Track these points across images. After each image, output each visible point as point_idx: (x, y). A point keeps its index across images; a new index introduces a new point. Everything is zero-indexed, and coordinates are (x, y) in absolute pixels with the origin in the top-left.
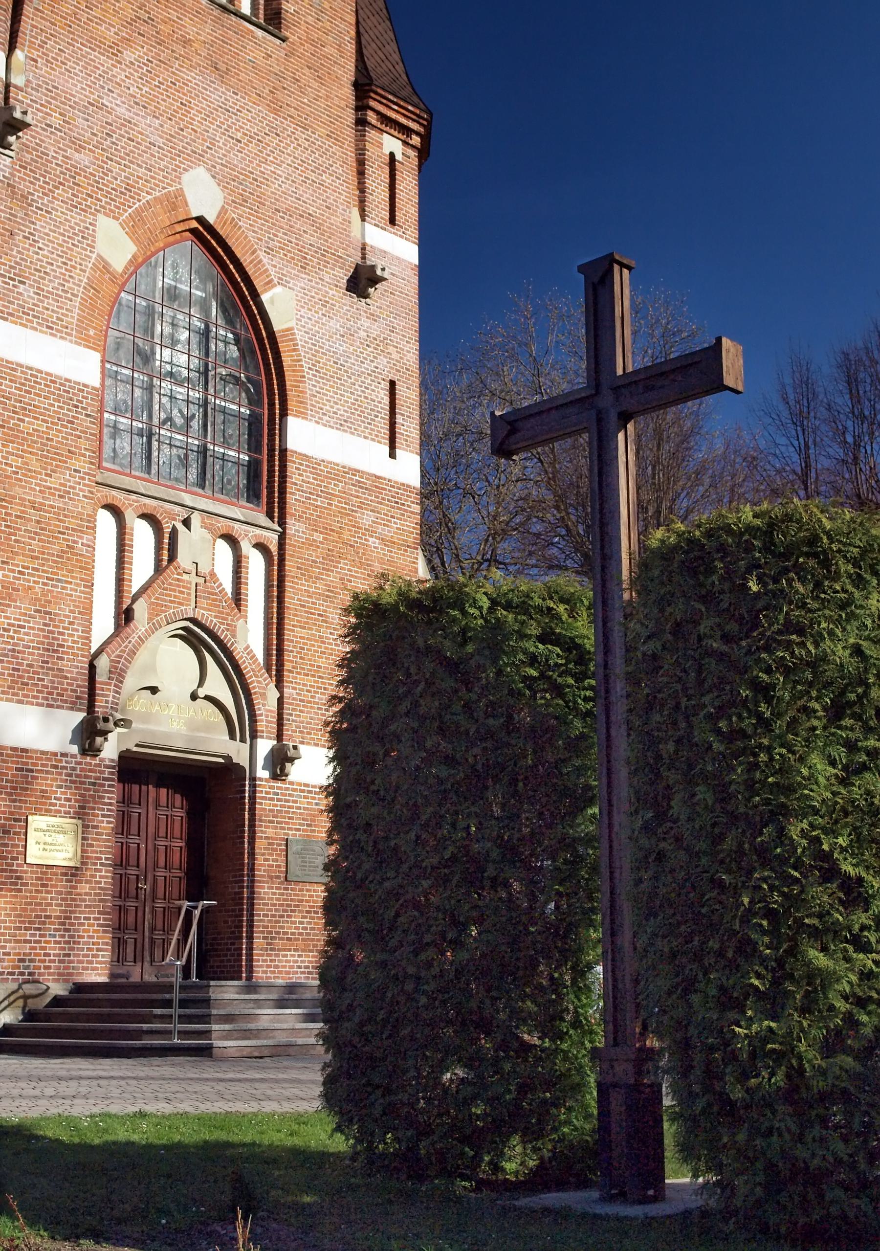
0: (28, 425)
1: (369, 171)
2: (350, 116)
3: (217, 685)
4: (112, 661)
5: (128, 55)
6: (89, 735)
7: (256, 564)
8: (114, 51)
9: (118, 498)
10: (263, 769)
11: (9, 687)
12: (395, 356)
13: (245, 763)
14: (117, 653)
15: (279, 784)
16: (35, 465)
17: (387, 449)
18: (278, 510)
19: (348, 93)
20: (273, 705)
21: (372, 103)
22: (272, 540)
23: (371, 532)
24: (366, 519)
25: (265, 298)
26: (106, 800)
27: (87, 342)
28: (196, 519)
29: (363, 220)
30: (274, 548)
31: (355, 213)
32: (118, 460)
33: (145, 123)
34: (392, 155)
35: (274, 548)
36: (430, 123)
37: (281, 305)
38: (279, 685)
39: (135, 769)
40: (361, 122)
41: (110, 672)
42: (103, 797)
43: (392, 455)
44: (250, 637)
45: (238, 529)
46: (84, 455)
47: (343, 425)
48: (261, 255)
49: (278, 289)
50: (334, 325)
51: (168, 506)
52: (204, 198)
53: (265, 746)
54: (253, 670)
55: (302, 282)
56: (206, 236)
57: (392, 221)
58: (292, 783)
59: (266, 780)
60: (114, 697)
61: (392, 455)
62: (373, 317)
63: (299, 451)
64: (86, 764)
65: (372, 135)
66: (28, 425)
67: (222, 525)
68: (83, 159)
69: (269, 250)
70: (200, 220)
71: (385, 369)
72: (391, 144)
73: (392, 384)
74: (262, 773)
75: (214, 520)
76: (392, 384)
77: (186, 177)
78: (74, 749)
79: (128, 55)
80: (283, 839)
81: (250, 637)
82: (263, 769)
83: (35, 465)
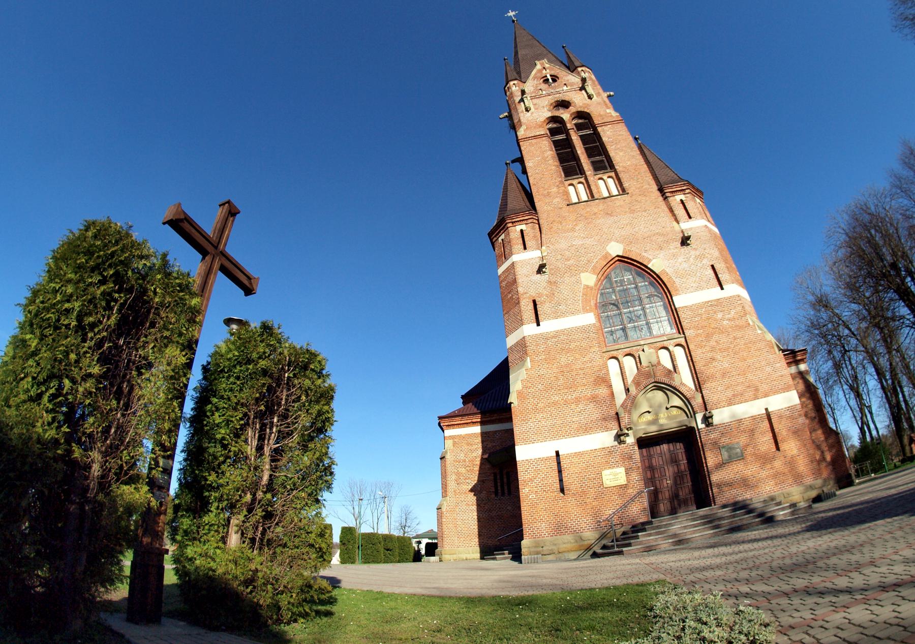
0: (573, 346)
1: (674, 209)
2: (661, 199)
3: (676, 401)
5: (577, 228)
6: (619, 437)
7: (679, 353)
8: (573, 230)
9: (614, 353)
16: (578, 356)
17: (719, 288)
19: (658, 193)
20: (700, 400)
22: (682, 341)
24: (720, 315)
27: (587, 311)
28: (646, 348)
30: (684, 343)
31: (675, 223)
32: (630, 339)
33: (588, 242)
34: (682, 201)
35: (684, 343)
36: (689, 183)
37: (656, 265)
38: (701, 392)
39: (644, 443)
40: (665, 198)
43: (722, 289)
44: (685, 379)
45: (666, 344)
47: (699, 288)
48: (644, 254)
49: (654, 261)
50: (680, 259)
52: (616, 249)
53: (699, 417)
55: (662, 254)
56: (624, 260)
57: (690, 217)
61: (722, 289)
65: (670, 199)
66: (573, 346)
67: (659, 345)
68: (571, 262)
70: (618, 256)
71: (707, 263)
72: (679, 197)
73: (712, 266)
74: (701, 426)
75: (655, 345)
76: (712, 266)
77: (608, 248)
78: (616, 443)
79: (577, 228)
81: (685, 379)
83: (578, 356)
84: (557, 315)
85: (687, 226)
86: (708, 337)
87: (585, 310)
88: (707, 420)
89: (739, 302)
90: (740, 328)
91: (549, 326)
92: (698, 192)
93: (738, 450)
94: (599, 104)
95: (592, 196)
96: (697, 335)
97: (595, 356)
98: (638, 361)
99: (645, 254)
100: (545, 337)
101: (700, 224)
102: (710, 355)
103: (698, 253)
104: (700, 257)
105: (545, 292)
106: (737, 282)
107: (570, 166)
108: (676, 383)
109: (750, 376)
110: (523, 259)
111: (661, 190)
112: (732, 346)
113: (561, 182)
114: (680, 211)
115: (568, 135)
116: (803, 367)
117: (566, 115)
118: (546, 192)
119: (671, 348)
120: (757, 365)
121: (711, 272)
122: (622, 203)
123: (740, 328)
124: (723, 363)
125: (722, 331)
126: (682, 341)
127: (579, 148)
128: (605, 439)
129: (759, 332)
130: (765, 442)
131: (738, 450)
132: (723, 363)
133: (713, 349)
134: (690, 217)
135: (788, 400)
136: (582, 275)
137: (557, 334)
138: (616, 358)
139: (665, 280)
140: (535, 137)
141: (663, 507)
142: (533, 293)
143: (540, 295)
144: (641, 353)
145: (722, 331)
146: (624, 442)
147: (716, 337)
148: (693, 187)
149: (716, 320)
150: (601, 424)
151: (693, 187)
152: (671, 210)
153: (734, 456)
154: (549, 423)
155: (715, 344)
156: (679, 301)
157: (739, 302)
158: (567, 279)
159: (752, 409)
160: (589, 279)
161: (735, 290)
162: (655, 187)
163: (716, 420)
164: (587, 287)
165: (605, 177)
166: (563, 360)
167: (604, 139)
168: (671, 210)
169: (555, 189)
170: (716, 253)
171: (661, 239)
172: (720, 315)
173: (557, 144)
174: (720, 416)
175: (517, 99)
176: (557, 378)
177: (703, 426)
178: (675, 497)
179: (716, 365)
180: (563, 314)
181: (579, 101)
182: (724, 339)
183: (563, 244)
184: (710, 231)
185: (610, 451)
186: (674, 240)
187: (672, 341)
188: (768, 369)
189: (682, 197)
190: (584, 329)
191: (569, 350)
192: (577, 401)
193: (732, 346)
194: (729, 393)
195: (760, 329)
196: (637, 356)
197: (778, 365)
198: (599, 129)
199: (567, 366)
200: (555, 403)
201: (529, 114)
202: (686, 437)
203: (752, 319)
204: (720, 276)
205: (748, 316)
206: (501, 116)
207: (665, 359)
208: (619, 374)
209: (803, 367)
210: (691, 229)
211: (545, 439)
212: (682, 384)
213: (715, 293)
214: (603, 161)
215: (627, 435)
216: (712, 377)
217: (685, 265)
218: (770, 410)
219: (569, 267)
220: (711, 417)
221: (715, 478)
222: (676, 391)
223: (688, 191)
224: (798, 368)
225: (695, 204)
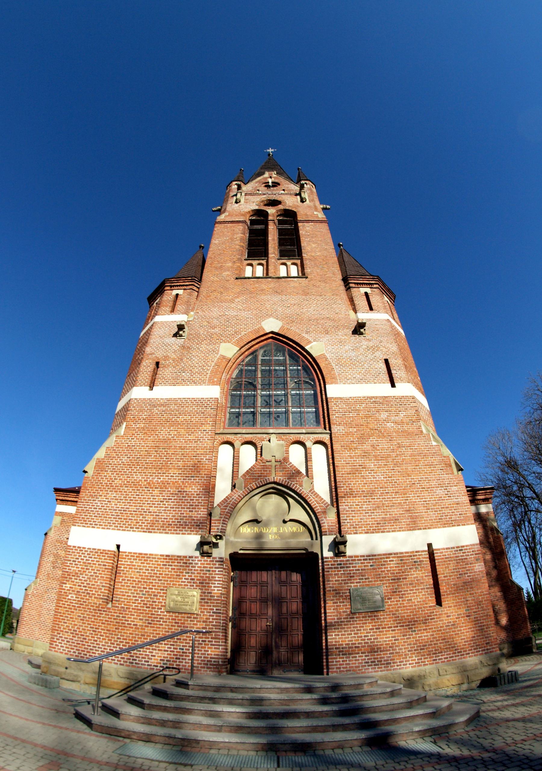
0: (181, 419)
4: (221, 509)
6: (205, 547)
7: (319, 454)
9: (231, 438)
10: (329, 551)
11: (161, 527)
12: (384, 350)
13: (317, 550)
14: (225, 504)
15: (342, 559)
18: (328, 424)
19: (342, 283)
21: (350, 281)
23: (387, 420)
24: (384, 415)
25: (307, 348)
26: (217, 579)
27: (213, 383)
29: (356, 312)
30: (328, 442)
31: (352, 313)
33: (244, 314)
34: (366, 294)
35: (328, 442)
36: (378, 277)
41: (221, 514)
42: (215, 577)
44: (320, 486)
45: (302, 438)
46: (209, 424)
47: (363, 380)
51: (259, 436)
52: (272, 325)
53: (328, 540)
54: (316, 501)
56: (278, 338)
57: (371, 309)
58: (350, 557)
59: (331, 558)
60: (222, 526)
61: (393, 385)
62: (369, 340)
63: (334, 396)
64: (204, 561)
65: (353, 290)
66: (181, 419)
67: (293, 438)
69: (307, 333)
70: (272, 332)
71: (381, 356)
72: (363, 290)
73: (386, 361)
74: (327, 554)
75: (287, 436)
76: (386, 361)
78: (197, 554)
80: (347, 589)
82: (329, 551)
84: (176, 382)
85: (363, 316)
86: (363, 439)
87: (212, 382)
88: (338, 546)
89: (413, 404)
90: (408, 434)
91: (162, 392)
92: (387, 291)
93: (378, 597)
94: (309, 207)
95: (267, 274)
96: (348, 434)
97: (204, 436)
98: (260, 452)
99: (306, 336)
100: (153, 403)
101: (381, 317)
102: (360, 461)
103: (371, 344)
104: (375, 349)
105: (174, 356)
106: (416, 385)
107: (256, 248)
108: (304, 490)
109: (413, 498)
110: (165, 319)
111: (345, 280)
112: (394, 454)
113: (240, 260)
114: (361, 302)
115: (267, 225)
116: (483, 509)
117: (271, 211)
118: (219, 265)
119: (308, 444)
120: (425, 484)
121: (384, 367)
122: (297, 285)
123: (408, 434)
124: (376, 474)
125: (382, 434)
126: (326, 438)
127: (273, 237)
128: (186, 543)
129: (434, 443)
130: (420, 596)
131: (378, 597)
132: (376, 474)
133: (366, 455)
134: (371, 309)
135: (469, 535)
136: (223, 345)
137: (168, 402)
138: (231, 444)
139: (322, 365)
140: (232, 222)
141: (250, 659)
142: (159, 355)
143: (166, 358)
144: (265, 443)
145: (382, 434)
146: (208, 555)
147: (373, 440)
148: (384, 284)
149: (377, 420)
150: (182, 526)
151: (384, 284)
152: (352, 300)
153: (367, 609)
154: (120, 506)
155: (369, 448)
156: (333, 391)
157: (413, 404)
158: (204, 347)
159: (407, 542)
160: (229, 350)
161: (408, 389)
162: (340, 277)
163: (350, 551)
164: (224, 357)
165: (289, 263)
166: (163, 433)
167: (301, 232)
168: (352, 300)
169: (230, 264)
170: (394, 348)
171: (329, 323)
172: (384, 415)
173: (252, 232)
174: (358, 544)
175: (232, 194)
176: (149, 454)
177: (331, 554)
178: (266, 652)
179: (367, 476)
180: (184, 382)
181: (290, 202)
182: (384, 444)
183: (215, 312)
184: (392, 326)
185: (184, 562)
186: (344, 327)
187: (312, 436)
188: (440, 492)
189: (368, 290)
190: (200, 403)
191: (176, 424)
192: (163, 486)
193: (394, 454)
194: (379, 515)
195: (436, 440)
196: (259, 447)
197: (454, 488)
198: (300, 224)
199: (165, 441)
200: (136, 484)
201: (237, 205)
202: (304, 565)
203: (427, 427)
204: (393, 372)
205: (422, 423)
206: (215, 209)
207: (296, 456)
208: (231, 463)
209: (483, 509)
210: (370, 320)
211: (107, 527)
212: (312, 491)
213: (383, 389)
214: (291, 247)
215: (216, 545)
216: (350, 494)
217: (353, 354)
218: (434, 547)
219: (211, 336)
220: (344, 543)
221: (334, 638)
222: (303, 502)
223: (375, 286)
224: (477, 509)
225: (379, 299)
